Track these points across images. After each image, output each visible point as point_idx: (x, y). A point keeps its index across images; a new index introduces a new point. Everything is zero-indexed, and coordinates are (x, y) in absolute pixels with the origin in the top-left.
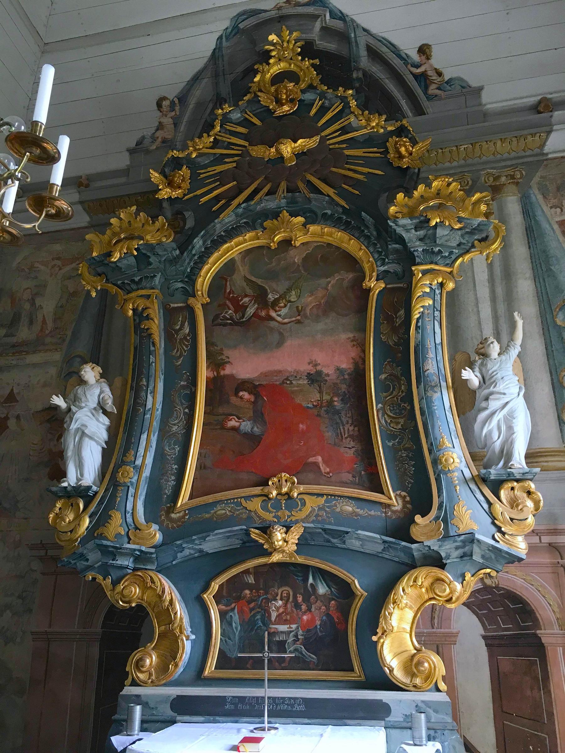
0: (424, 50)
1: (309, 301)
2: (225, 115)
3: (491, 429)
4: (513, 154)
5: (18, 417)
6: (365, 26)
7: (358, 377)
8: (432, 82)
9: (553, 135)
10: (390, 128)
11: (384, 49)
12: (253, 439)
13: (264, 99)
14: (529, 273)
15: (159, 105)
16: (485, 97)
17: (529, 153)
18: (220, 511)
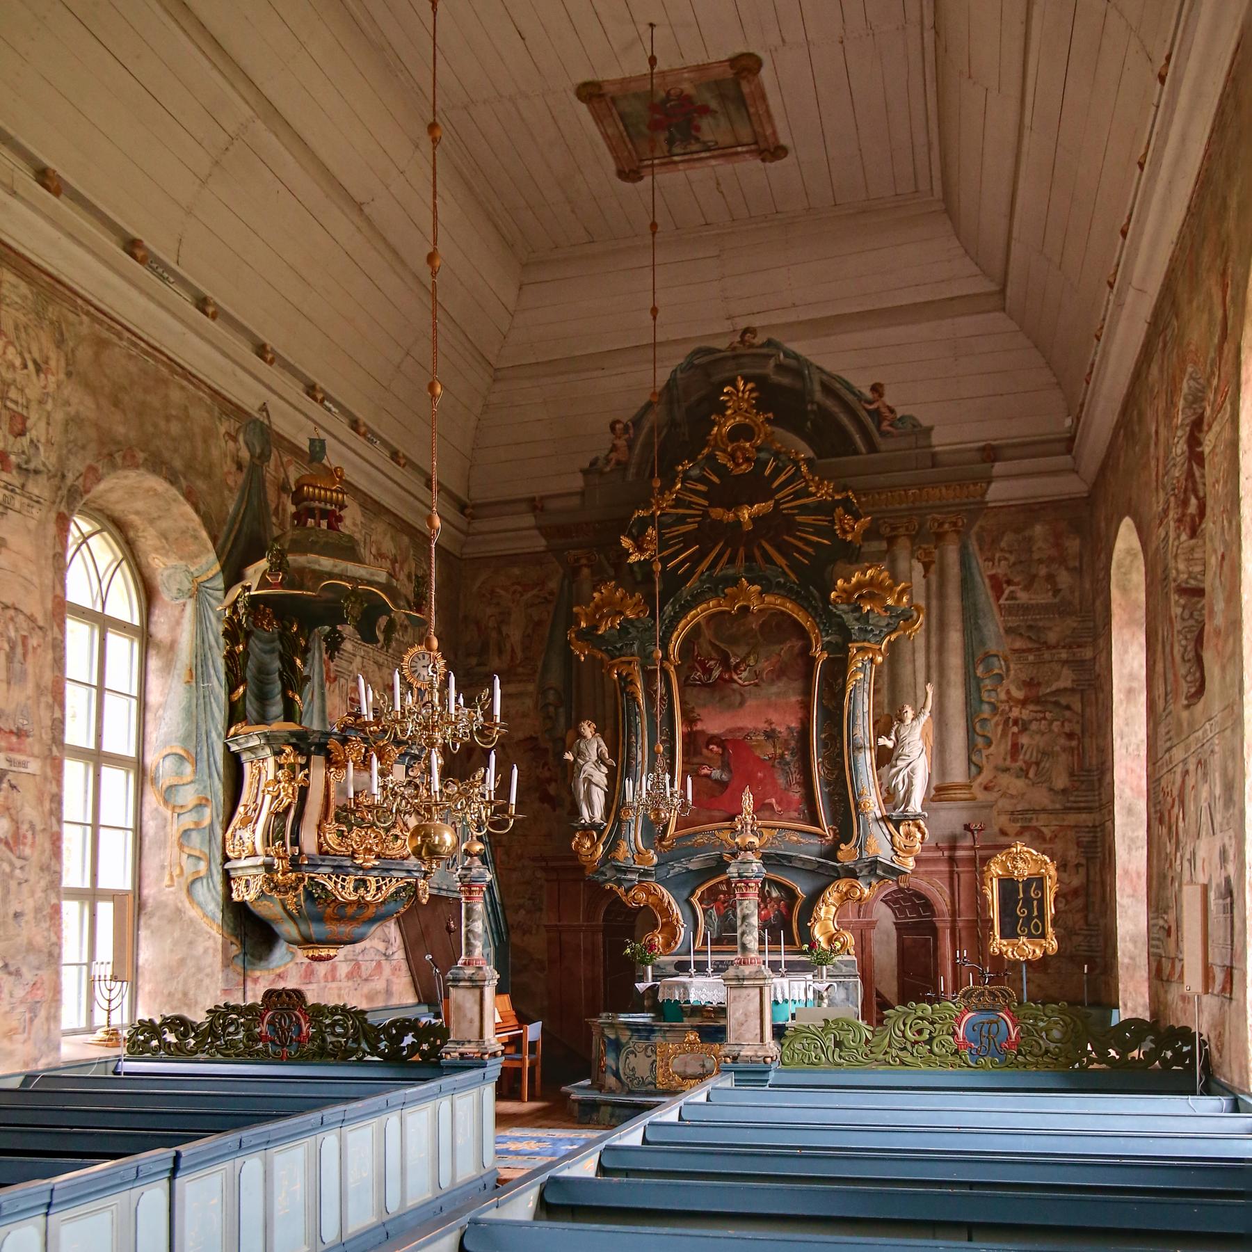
0: (877, 389)
1: (765, 665)
2: (685, 472)
4: (957, 501)
6: (819, 364)
8: (885, 419)
9: (993, 485)
10: (837, 497)
11: (838, 386)
13: (721, 458)
14: (959, 626)
15: (613, 428)
16: (935, 439)
17: (971, 500)
18: (700, 839)
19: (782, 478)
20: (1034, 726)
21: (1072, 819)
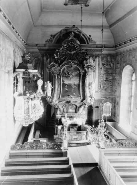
0: (90, 36)
3: (91, 92)
5: (31, 81)
7: (79, 85)
12: (67, 91)
19: (77, 48)
20: (106, 84)
21: (110, 96)
